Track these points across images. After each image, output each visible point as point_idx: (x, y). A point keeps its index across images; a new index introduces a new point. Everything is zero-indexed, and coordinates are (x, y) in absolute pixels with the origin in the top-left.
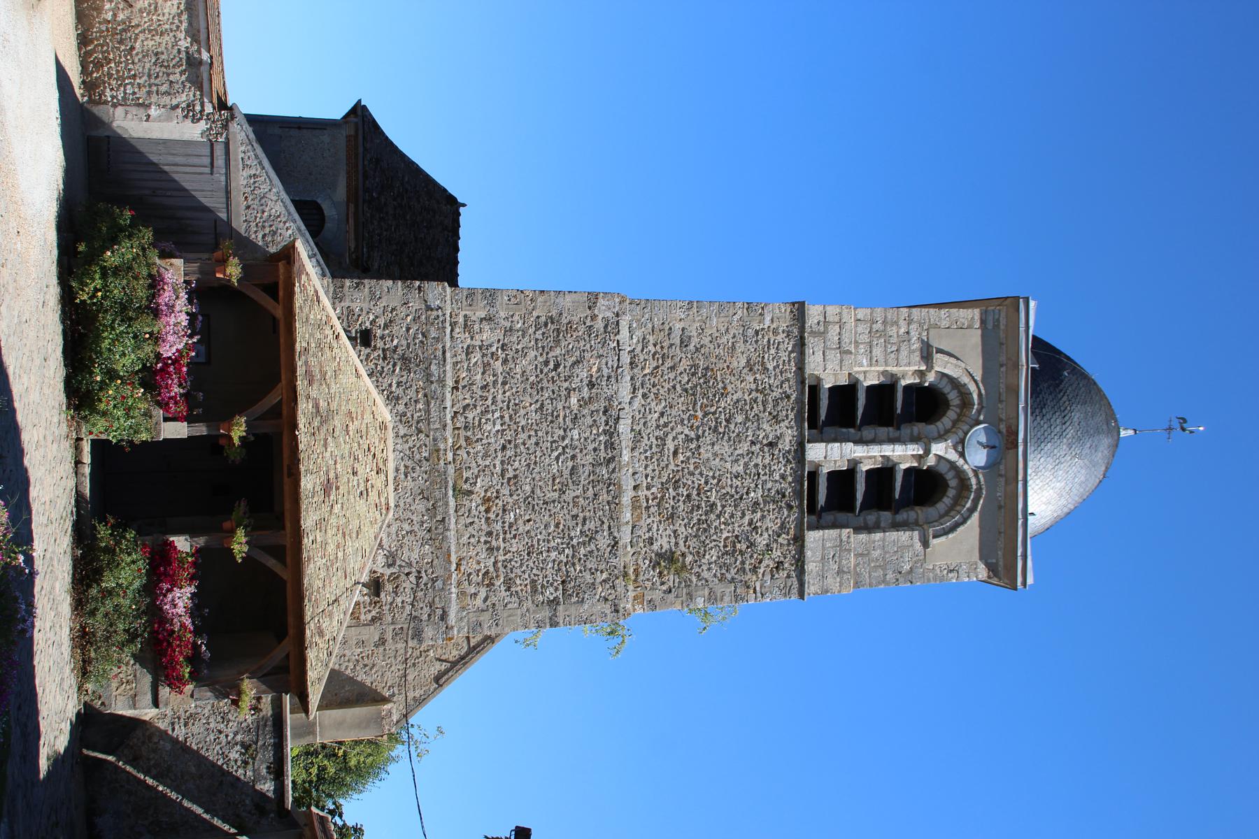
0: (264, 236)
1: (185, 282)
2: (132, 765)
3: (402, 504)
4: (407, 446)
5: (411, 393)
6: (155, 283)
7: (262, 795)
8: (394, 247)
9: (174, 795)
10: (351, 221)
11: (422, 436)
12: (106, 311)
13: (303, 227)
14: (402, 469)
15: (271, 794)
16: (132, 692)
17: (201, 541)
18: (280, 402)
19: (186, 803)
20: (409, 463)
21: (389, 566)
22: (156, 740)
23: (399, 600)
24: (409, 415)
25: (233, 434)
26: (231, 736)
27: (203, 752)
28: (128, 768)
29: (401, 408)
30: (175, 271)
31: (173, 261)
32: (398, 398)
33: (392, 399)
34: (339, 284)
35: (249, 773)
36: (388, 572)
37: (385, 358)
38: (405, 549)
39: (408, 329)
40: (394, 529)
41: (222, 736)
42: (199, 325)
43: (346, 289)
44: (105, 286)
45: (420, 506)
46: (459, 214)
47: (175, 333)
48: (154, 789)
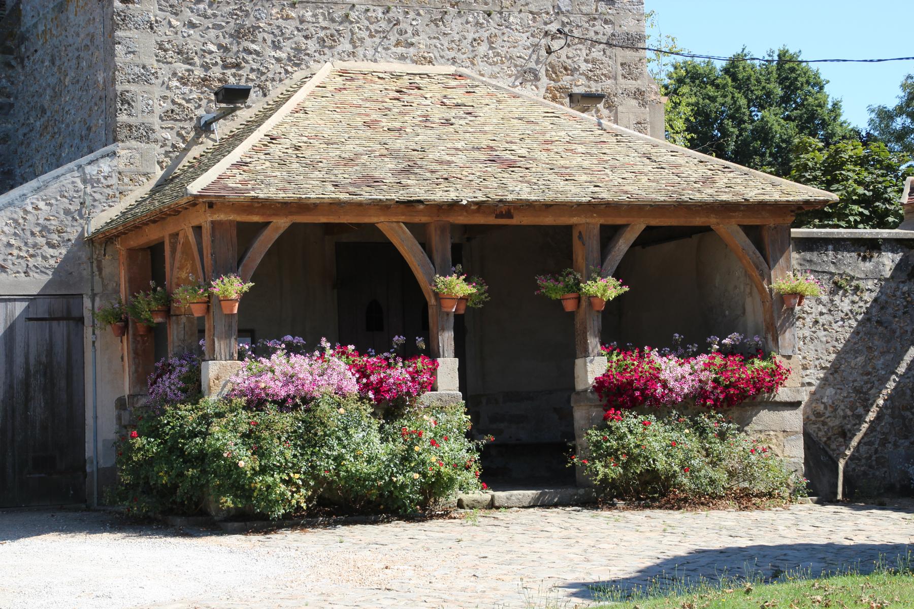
0: (50, 245)
2: (851, 439)
3: (452, 54)
4: (368, 41)
5: (290, 27)
7: (898, 268)
9: (891, 385)
11: (353, 15)
12: (313, 467)
13: (33, 183)
14: (400, 50)
15: (898, 257)
16: (780, 435)
17: (593, 342)
18: (411, 226)
19: (902, 369)
21: (537, 78)
22: (822, 407)
23: (584, 67)
24: (322, 34)
25: (460, 294)
26: (821, 308)
27: (840, 346)
28: (854, 443)
29: (312, 46)
32: (298, 49)
33: (298, 58)
34: (126, 131)
35: (870, 284)
36: (544, 81)
37: (238, 66)
38: (515, 52)
39: (192, 25)
40: (487, 69)
41: (822, 320)
43: (132, 121)
44: (281, 469)
47: (330, 373)
48: (881, 410)
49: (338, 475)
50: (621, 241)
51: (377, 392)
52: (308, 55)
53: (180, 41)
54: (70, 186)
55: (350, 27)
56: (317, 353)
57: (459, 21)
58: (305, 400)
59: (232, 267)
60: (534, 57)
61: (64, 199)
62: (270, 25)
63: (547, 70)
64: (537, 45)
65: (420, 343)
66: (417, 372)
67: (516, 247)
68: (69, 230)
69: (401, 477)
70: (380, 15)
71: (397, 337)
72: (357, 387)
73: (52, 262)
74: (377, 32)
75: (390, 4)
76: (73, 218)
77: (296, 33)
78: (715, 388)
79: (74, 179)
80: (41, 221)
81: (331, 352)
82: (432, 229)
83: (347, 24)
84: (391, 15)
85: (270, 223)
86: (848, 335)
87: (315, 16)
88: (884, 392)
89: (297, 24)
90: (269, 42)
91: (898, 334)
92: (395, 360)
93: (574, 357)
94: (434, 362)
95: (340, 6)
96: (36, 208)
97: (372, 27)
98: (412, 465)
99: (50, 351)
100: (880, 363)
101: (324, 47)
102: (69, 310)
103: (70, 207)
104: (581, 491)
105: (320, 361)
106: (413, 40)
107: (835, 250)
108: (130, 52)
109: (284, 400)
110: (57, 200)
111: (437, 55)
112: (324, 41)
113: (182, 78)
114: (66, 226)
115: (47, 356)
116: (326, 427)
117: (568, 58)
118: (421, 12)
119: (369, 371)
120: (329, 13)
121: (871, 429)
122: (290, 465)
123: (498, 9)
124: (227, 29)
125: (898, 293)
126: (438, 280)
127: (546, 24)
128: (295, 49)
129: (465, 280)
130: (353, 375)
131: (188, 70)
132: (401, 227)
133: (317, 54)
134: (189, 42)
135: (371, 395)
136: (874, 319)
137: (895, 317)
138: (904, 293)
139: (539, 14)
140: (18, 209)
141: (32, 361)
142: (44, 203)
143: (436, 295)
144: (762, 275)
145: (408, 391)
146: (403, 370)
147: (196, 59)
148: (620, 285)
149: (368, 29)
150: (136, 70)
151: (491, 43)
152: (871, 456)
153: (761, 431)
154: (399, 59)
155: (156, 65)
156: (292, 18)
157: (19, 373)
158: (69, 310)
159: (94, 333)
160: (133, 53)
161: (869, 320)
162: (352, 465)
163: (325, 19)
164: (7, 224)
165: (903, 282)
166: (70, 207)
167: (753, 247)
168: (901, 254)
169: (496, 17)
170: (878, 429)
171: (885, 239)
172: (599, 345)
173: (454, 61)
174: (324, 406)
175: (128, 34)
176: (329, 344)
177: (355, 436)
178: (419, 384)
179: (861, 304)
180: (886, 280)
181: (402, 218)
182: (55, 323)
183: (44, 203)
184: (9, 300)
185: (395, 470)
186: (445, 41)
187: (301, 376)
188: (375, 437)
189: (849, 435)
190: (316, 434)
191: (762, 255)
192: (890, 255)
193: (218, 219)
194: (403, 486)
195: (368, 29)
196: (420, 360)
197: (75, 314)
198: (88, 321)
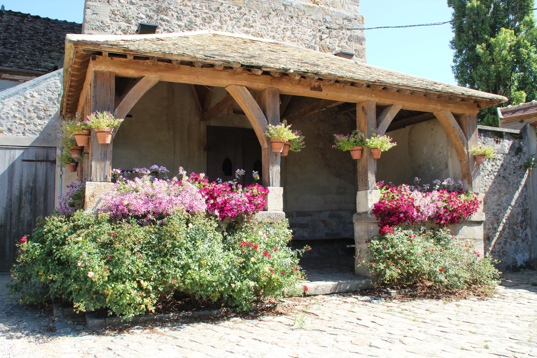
0: (39, 118)
1: (114, 181)
3: (273, 34)
4: (229, 22)
5: (187, 10)
6: (119, 215)
7: (512, 148)
8: (37, 53)
9: (509, 211)
10: (16, 77)
11: (221, 9)
12: (163, 274)
14: (246, 29)
15: (511, 142)
19: (513, 203)
20: (243, 22)
24: (204, 16)
28: (493, 243)
29: (199, 21)
30: (101, 191)
31: (88, 193)
32: (191, 22)
38: (304, 37)
42: (163, 169)
45: (274, 20)
46: (10, 11)
47: (184, 194)
49: (183, 282)
50: (388, 115)
51: (221, 211)
52: (196, 25)
53: (124, 10)
54: (53, 85)
55: (220, 14)
56: (175, 179)
57: (277, 18)
58: (161, 216)
59: (112, 108)
60: (314, 41)
61: (49, 92)
62: (176, 8)
63: (320, 48)
64: (315, 35)
65: (256, 175)
66: (253, 196)
67: (325, 113)
68: (50, 109)
69: (239, 284)
70: (236, 10)
71: (238, 170)
72: (206, 206)
73: (39, 127)
74: (234, 18)
75: (242, 6)
76: (54, 103)
77: (190, 13)
78: (445, 212)
79: (55, 81)
80: (35, 104)
81: (187, 178)
82: (267, 93)
83: (218, 12)
84: (241, 11)
85: (143, 77)
86: (490, 184)
87: (200, 6)
88: (506, 215)
89: (191, 9)
90: (175, 17)
91: (511, 184)
92: (237, 186)
93: (356, 190)
94: (265, 189)
95: (215, 3)
96: (32, 96)
97: (232, 16)
98: (249, 272)
99: (35, 181)
100: (504, 199)
101: (206, 22)
102: (47, 156)
103: (53, 96)
104: (363, 282)
105: (177, 185)
106: (253, 25)
107: (484, 136)
108: (95, 14)
109: (145, 216)
110: (45, 92)
111: (265, 34)
112: (205, 19)
113: (124, 30)
114: (49, 107)
115: (33, 183)
116: (175, 240)
117: (330, 43)
118: (258, 11)
119: (216, 194)
120: (209, 6)
121: (500, 235)
122: (142, 273)
123: (296, 15)
124: (152, 8)
125: (511, 162)
126: (270, 129)
127: (319, 26)
128: (189, 22)
129: (290, 129)
130: (203, 196)
131: (128, 27)
132: (244, 89)
133: (201, 26)
134: (130, 12)
135: (217, 213)
136: (502, 175)
137: (510, 174)
138: (513, 162)
139: (316, 21)
140: (21, 96)
141: (24, 185)
142: (37, 93)
143: (269, 140)
144: (463, 144)
145: (246, 210)
146: (243, 195)
147: (133, 21)
148: (391, 142)
149: (229, 16)
150: (98, 23)
151: (292, 31)
152: (500, 251)
153: (463, 239)
154: (245, 33)
155: (109, 21)
156: (188, 6)
157: (16, 192)
158: (47, 156)
159: (61, 170)
160: (96, 14)
161: (499, 175)
162: (197, 274)
163: (206, 8)
164: (14, 105)
165: (513, 156)
166: (53, 96)
167: (459, 127)
168: (512, 141)
169: (295, 19)
170: (503, 235)
171: (506, 133)
172: (375, 182)
173: (274, 38)
174: (176, 222)
175: (94, 4)
176: (185, 172)
177: (201, 247)
178: (254, 205)
179: (496, 167)
180: (506, 154)
181: (245, 83)
182: (39, 163)
183: (37, 93)
184: (12, 149)
185: (234, 277)
186: (269, 27)
187: (160, 196)
188: (218, 248)
189: (491, 239)
190: (165, 246)
191: (463, 131)
192: (507, 141)
193: (100, 70)
194: (241, 291)
195: (229, 16)
196: (255, 187)
197: (51, 159)
198: (58, 163)
